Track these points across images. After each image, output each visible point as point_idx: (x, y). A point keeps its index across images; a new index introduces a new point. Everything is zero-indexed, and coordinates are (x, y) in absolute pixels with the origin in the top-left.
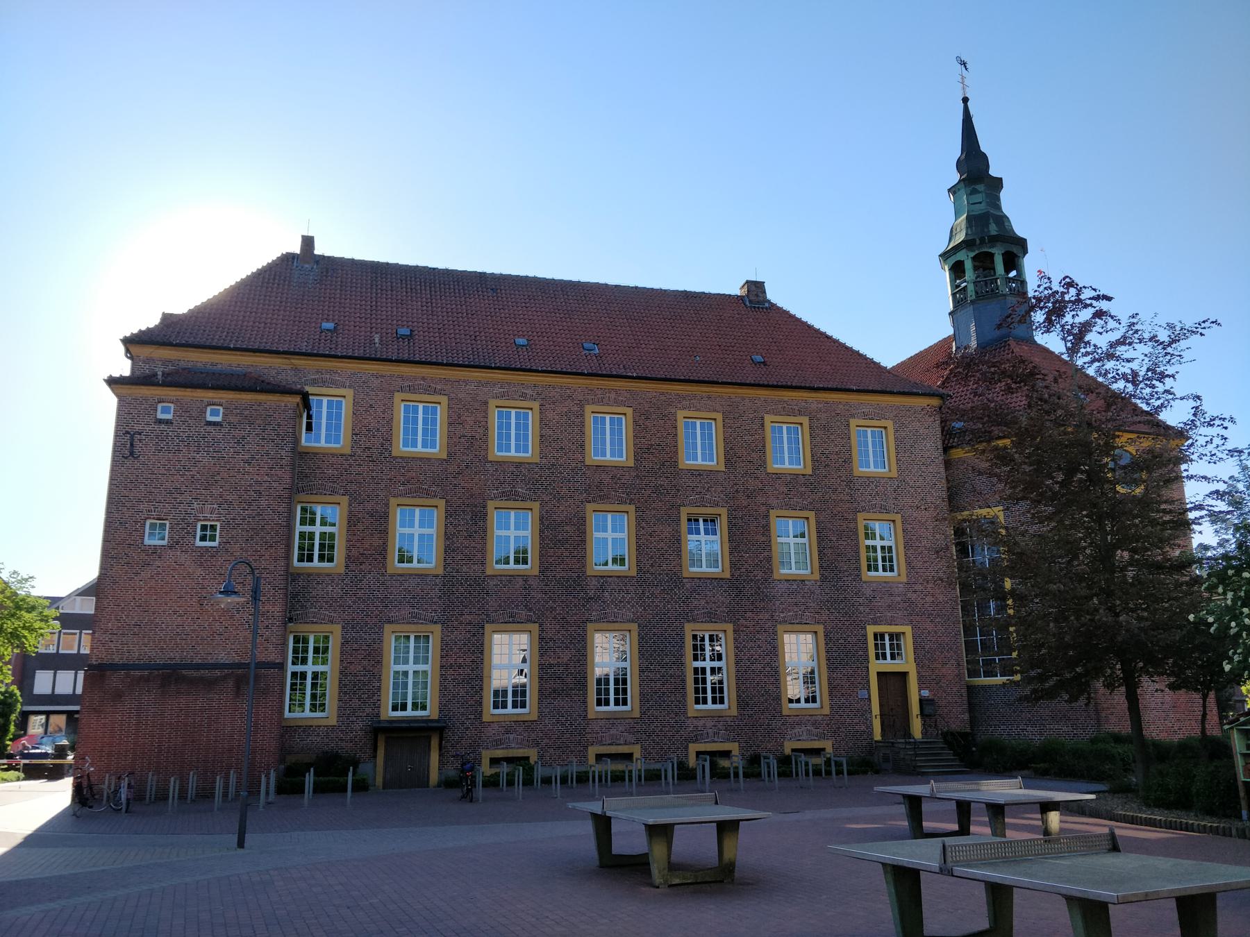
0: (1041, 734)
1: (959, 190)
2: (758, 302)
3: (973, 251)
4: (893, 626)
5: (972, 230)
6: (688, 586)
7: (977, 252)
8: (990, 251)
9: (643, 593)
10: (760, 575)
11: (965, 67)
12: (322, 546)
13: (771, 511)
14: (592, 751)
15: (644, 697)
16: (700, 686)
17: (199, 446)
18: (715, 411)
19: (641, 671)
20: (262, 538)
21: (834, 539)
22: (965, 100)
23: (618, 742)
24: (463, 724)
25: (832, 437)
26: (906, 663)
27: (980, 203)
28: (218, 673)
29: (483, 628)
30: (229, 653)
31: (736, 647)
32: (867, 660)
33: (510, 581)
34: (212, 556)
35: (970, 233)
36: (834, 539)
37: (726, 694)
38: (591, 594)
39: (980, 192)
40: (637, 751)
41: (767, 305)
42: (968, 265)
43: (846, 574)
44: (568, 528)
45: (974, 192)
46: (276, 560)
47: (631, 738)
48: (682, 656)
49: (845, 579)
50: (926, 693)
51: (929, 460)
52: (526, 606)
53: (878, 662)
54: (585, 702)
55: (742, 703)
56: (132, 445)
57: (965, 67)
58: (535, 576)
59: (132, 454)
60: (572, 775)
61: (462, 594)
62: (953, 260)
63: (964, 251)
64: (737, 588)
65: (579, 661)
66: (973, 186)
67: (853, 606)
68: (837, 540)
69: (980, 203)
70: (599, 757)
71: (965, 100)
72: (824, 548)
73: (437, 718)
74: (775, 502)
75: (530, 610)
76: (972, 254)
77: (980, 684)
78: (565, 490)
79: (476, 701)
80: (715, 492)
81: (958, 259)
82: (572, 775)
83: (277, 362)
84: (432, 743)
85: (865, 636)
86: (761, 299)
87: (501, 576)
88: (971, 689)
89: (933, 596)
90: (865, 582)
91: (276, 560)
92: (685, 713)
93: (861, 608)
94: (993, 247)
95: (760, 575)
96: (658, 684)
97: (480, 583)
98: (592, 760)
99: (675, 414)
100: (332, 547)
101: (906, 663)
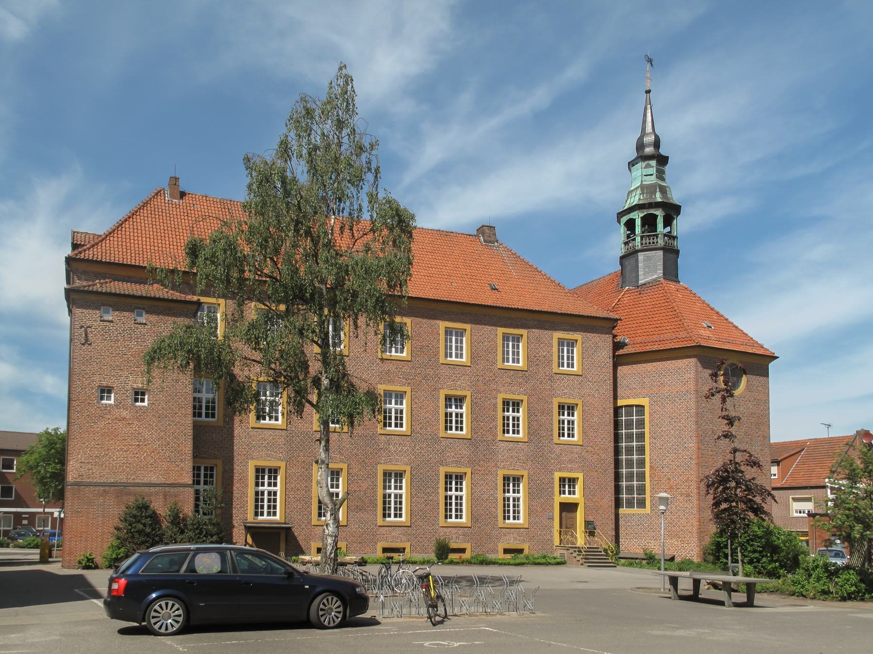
5: (643, 196)
6: (443, 443)
7: (645, 213)
9: (415, 446)
10: (490, 437)
11: (651, 63)
12: (207, 408)
15: (412, 513)
17: (131, 338)
20: (176, 401)
24: (300, 526)
25: (542, 345)
26: (577, 496)
27: (652, 175)
28: (153, 489)
30: (158, 477)
34: (144, 413)
38: (381, 446)
42: (638, 222)
43: (545, 438)
46: (185, 416)
47: (404, 538)
48: (438, 488)
51: (603, 364)
52: (339, 452)
55: (474, 517)
56: (86, 335)
57: (651, 63)
59: (87, 340)
60: (475, 578)
61: (299, 442)
62: (624, 219)
64: (475, 445)
65: (373, 489)
67: (547, 459)
68: (541, 416)
69: (652, 175)
72: (532, 421)
75: (342, 455)
76: (642, 215)
79: (308, 512)
80: (464, 380)
82: (475, 578)
83: (650, 124)
84: (281, 537)
85: (437, 475)
89: (598, 455)
91: (185, 416)
95: (490, 437)
100: (213, 408)
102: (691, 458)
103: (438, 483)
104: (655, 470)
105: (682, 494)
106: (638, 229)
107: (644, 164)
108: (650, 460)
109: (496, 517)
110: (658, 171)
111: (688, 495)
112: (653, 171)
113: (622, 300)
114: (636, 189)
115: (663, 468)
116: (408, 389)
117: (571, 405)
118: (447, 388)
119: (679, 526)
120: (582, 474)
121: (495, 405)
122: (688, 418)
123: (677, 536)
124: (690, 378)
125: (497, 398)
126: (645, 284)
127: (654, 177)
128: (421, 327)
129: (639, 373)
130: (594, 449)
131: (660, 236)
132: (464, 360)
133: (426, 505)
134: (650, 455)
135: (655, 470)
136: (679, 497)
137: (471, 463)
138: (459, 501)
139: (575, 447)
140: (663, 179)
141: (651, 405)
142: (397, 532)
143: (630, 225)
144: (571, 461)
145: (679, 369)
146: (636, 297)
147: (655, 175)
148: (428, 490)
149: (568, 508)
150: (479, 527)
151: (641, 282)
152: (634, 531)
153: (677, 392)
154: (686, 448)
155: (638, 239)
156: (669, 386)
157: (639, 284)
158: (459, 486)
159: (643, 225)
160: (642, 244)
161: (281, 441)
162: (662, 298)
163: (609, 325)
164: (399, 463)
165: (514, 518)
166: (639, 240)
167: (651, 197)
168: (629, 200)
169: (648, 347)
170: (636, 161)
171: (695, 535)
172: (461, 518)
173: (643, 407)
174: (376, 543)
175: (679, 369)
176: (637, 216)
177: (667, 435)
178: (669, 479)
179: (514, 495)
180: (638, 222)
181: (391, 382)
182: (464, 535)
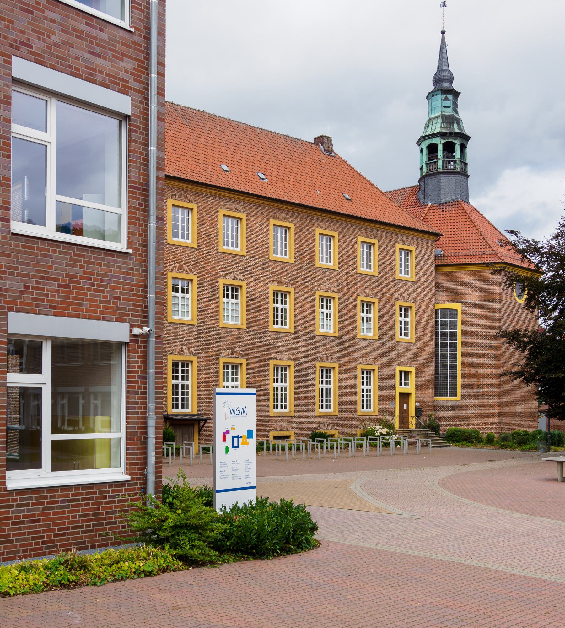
0: (468, 427)
1: (436, 95)
2: (329, 151)
3: (445, 140)
4: (408, 367)
5: (444, 125)
6: (318, 340)
7: (446, 140)
8: (454, 141)
13: (358, 297)
14: (273, 434)
16: (448, 386)
18: (334, 231)
19: (295, 390)
21: (385, 316)
22: (443, 32)
23: (284, 429)
25: (388, 254)
26: (411, 388)
27: (449, 107)
29: (218, 360)
31: (339, 377)
32: (395, 386)
33: (231, 332)
35: (443, 127)
36: (385, 316)
37: (372, 399)
38: (272, 342)
39: (450, 100)
40: (292, 434)
41: (333, 154)
42: (440, 148)
44: (260, 300)
45: (446, 99)
47: (289, 427)
48: (314, 381)
49: (389, 339)
50: (418, 404)
53: (401, 387)
54: (268, 407)
58: (244, 329)
62: (428, 142)
63: (439, 138)
66: (445, 95)
69: (449, 107)
70: (275, 437)
71: (443, 32)
73: (196, 413)
74: (360, 292)
75: (242, 350)
76: (443, 142)
77: (438, 400)
78: (259, 275)
81: (434, 142)
85: (314, 369)
86: (331, 149)
87: (227, 328)
88: (437, 403)
89: (425, 351)
90: (397, 342)
92: (314, 414)
93: (395, 357)
94: (455, 139)
96: (303, 397)
97: (216, 331)
98: (271, 438)
99: (314, 231)
101: (411, 388)
102: (495, 355)
103: (314, 376)
104: (466, 364)
105: (487, 385)
106: (440, 154)
107: (443, 97)
108: (462, 355)
109: (356, 407)
110: (453, 103)
111: (492, 385)
112: (449, 104)
113: (428, 215)
114: (437, 117)
115: (472, 362)
116: (292, 290)
117: (284, 293)
118: (321, 290)
119: (484, 411)
120: (377, 366)
121: (356, 306)
122: (493, 321)
123: (482, 419)
124: (495, 289)
125: (356, 300)
126: (446, 203)
127: (451, 109)
128: (301, 232)
129: (454, 282)
130: (422, 346)
131: (457, 162)
132: (190, 241)
133: (306, 397)
134: (462, 352)
135: (466, 364)
136: (484, 387)
137: (338, 359)
138: (284, 392)
139: (410, 344)
140: (456, 112)
141: (463, 309)
142: (284, 422)
143: (433, 149)
144: (407, 357)
145: (487, 280)
146: (440, 214)
147: (451, 107)
148: (307, 384)
149: (405, 396)
150: (344, 416)
151: (443, 201)
152: (447, 415)
153: (485, 300)
154: (491, 346)
155: (440, 162)
156: (479, 294)
157: (441, 203)
158: (235, 377)
159: (444, 150)
160: (443, 167)
161: (193, 337)
162: (463, 217)
163: (434, 238)
164: (285, 359)
165: (183, 407)
166: (441, 164)
167: (450, 128)
168: (430, 126)
169: (461, 260)
170: (436, 93)
171: (496, 418)
172: (330, 408)
173: (457, 310)
174: (269, 432)
175: (487, 280)
176: (440, 142)
177: (476, 336)
178: (477, 372)
179: (183, 381)
180: (440, 148)
181: (279, 282)
182: (333, 423)
